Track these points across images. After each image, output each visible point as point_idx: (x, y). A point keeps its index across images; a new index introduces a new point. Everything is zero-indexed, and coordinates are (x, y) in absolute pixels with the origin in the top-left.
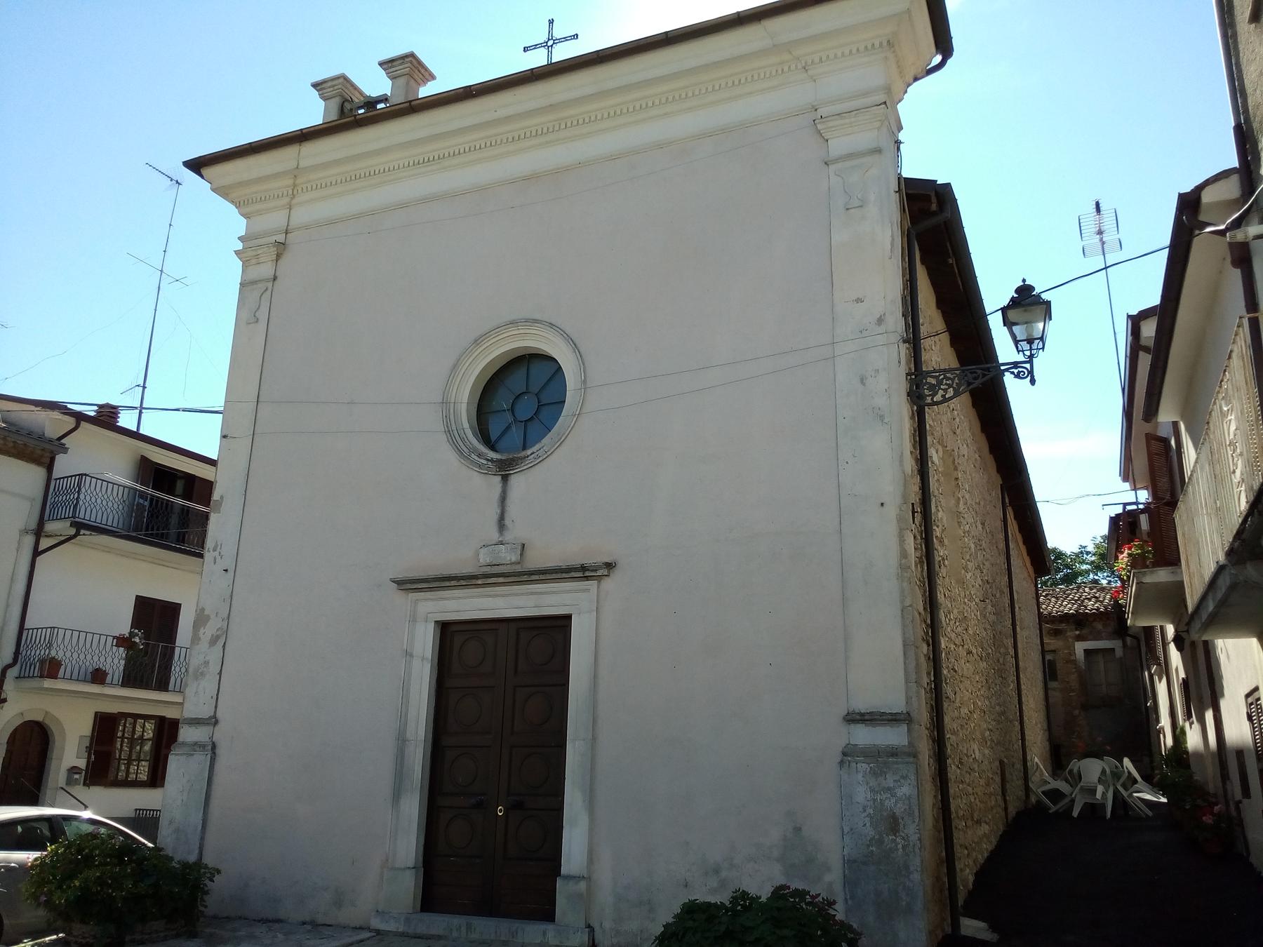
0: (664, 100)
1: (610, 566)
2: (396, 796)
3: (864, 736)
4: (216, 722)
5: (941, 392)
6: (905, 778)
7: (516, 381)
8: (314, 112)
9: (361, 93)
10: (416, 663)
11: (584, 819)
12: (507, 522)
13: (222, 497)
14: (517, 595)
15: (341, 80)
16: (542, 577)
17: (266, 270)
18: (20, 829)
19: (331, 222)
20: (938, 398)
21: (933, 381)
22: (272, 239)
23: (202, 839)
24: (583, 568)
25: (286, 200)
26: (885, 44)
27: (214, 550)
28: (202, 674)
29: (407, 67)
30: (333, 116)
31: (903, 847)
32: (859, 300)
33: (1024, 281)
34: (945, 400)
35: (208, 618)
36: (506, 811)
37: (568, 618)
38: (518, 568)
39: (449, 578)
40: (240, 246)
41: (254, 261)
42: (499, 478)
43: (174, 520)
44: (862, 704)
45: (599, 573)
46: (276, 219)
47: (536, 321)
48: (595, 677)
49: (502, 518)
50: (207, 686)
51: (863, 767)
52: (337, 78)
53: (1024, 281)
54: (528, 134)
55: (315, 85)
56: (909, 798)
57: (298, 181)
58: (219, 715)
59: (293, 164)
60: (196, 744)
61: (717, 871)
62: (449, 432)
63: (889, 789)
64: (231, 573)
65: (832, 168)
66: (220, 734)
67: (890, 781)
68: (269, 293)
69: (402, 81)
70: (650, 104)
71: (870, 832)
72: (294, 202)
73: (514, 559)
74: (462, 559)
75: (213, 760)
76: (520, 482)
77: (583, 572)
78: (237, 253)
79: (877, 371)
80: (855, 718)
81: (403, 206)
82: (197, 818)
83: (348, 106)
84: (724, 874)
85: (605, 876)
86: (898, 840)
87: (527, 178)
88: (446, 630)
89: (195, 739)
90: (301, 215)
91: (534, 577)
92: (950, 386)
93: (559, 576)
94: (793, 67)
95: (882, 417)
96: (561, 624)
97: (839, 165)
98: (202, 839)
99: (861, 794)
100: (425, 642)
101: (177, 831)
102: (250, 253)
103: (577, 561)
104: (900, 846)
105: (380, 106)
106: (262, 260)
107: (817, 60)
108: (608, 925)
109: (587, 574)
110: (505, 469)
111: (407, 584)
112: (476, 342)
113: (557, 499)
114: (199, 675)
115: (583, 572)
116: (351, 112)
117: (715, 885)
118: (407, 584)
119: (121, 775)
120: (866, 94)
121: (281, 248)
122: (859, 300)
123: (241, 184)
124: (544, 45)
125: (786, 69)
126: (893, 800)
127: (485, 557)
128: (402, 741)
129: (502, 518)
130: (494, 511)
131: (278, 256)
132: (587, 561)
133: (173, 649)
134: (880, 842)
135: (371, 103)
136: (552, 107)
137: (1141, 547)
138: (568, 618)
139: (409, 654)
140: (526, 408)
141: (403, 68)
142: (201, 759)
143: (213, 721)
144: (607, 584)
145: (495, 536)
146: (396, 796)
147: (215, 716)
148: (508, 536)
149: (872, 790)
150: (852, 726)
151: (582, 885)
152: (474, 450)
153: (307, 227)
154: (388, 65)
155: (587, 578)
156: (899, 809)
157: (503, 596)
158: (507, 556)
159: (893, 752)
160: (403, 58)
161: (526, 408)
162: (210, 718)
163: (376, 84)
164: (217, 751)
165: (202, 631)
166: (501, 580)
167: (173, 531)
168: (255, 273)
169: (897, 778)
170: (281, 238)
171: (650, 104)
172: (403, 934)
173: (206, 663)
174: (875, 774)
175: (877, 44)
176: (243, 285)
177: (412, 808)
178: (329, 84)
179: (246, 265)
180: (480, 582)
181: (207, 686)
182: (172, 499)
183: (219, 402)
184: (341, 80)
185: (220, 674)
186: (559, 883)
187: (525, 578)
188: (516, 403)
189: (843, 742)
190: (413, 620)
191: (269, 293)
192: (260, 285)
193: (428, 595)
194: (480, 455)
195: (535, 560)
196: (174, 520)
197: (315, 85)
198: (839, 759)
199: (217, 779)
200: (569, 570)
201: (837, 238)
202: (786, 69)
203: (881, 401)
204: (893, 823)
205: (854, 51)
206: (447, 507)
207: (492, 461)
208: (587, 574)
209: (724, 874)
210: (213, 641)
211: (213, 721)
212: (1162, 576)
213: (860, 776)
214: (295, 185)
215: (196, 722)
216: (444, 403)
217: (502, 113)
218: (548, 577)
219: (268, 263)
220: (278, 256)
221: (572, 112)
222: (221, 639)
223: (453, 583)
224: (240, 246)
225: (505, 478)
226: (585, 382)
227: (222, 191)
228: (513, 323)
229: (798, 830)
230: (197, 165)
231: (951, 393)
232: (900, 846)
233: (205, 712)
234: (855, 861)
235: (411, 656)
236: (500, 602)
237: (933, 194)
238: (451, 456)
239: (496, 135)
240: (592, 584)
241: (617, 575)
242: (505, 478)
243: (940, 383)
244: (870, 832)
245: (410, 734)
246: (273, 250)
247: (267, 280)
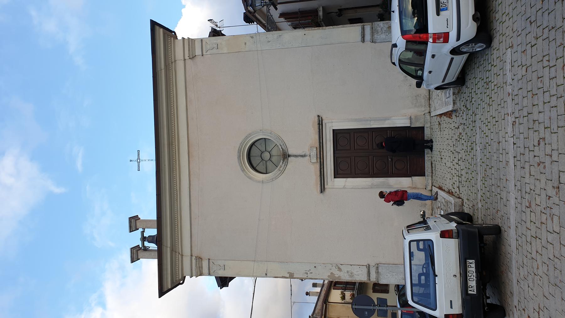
1: (318, 116)
3: (368, 37)
7: (255, 151)
12: (303, 154)
18: (366, 313)
24: (319, 124)
32: (245, 44)
38: (318, 148)
44: (359, 38)
49: (302, 156)
51: (376, 36)
65: (204, 53)
77: (320, 123)
80: (363, 40)
88: (337, 175)
89: (374, 273)
100: (341, 182)
108: (423, 109)
110: (286, 156)
111: (323, 189)
114: (352, 275)
115: (320, 123)
118: (323, 189)
119: (348, 294)
127: (314, 160)
129: (302, 156)
130: (300, 159)
139: (344, 188)
145: (308, 158)
148: (308, 153)
172: (432, 177)
174: (378, 33)
186: (413, 126)
201: (225, 52)
203: (275, 36)
210: (340, 269)
211: (368, 267)
225: (289, 156)
233: (365, 270)
236: (328, 143)
242: (289, 156)
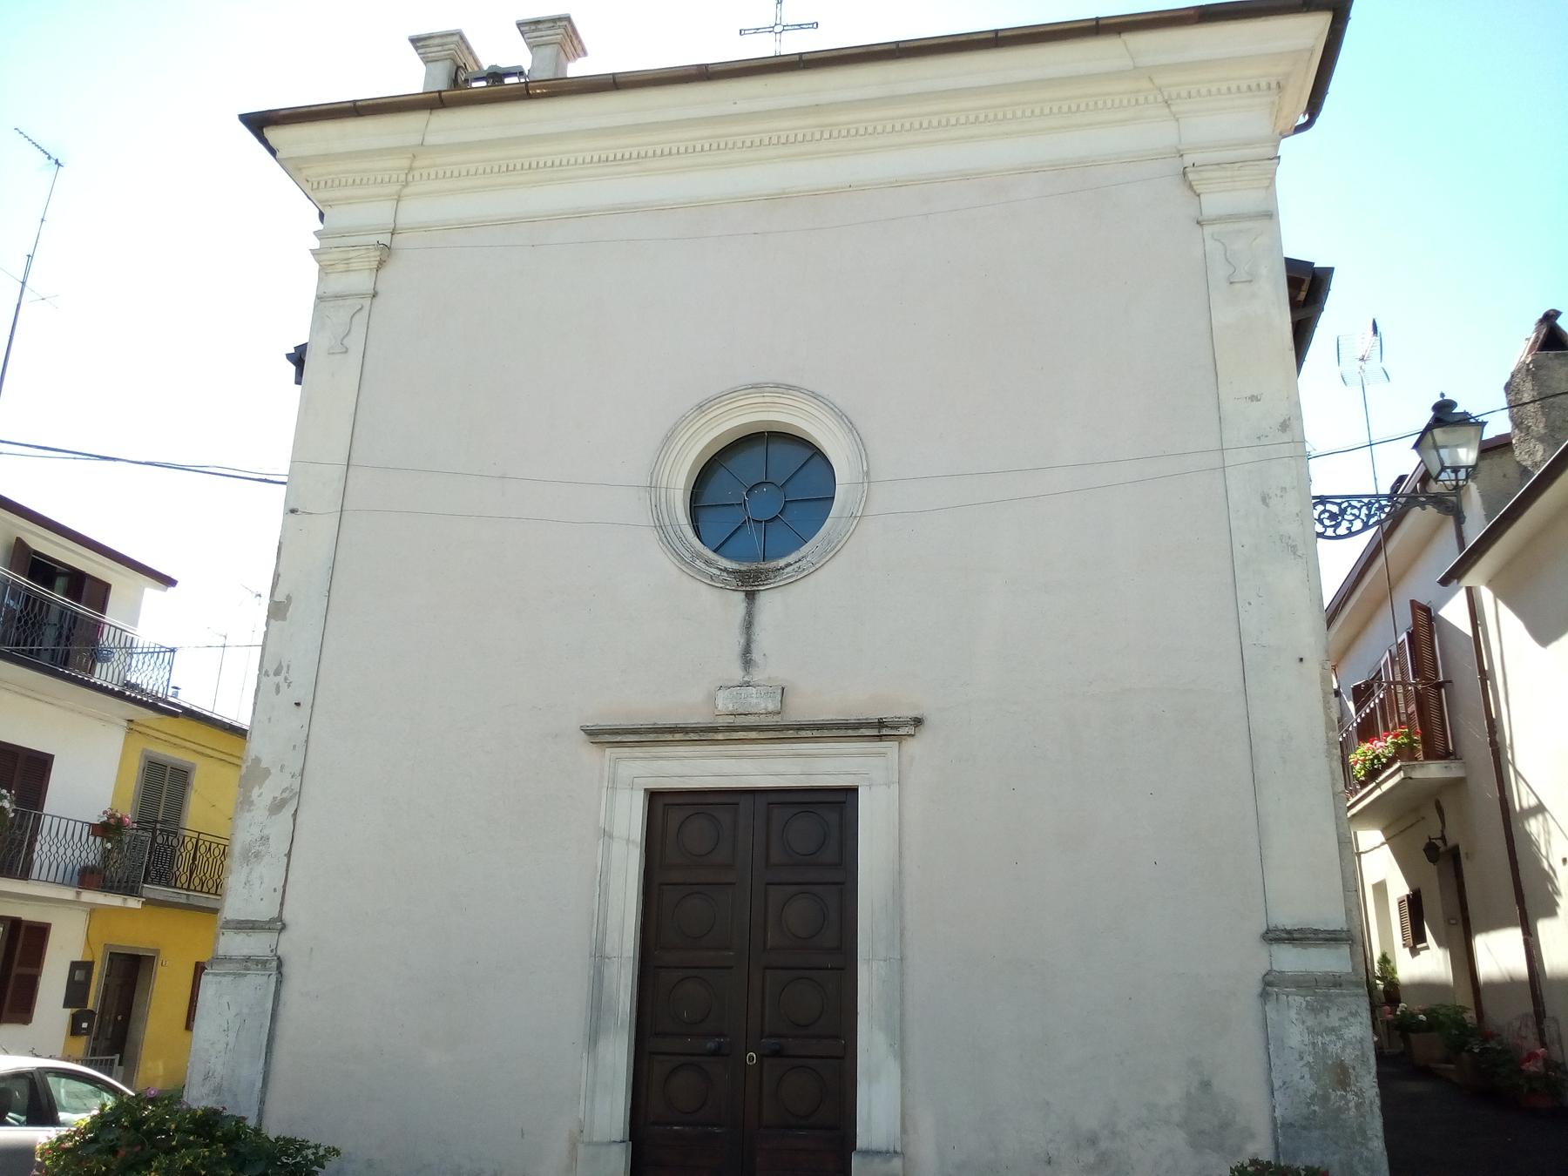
0: (972, 119)
1: (918, 722)
2: (593, 1037)
3: (1291, 960)
4: (284, 927)
5: (1345, 524)
6: (1354, 1014)
8: (411, 78)
9: (476, 61)
10: (618, 848)
11: (892, 1068)
12: (756, 655)
13: (289, 598)
14: (775, 756)
15: (456, 38)
16: (816, 733)
17: (360, 281)
19: (465, 226)
20: (1342, 530)
21: (1335, 509)
22: (373, 239)
23: (262, 1102)
24: (881, 724)
25: (395, 188)
26: (1274, 85)
27: (277, 673)
28: (257, 855)
29: (552, 32)
30: (441, 84)
31: (1358, 1106)
32: (1254, 398)
33: (1442, 395)
34: (1351, 534)
35: (267, 772)
36: (761, 1057)
37: (852, 791)
39: (673, 730)
40: (316, 244)
41: (341, 267)
42: (742, 595)
43: (50, 633)
44: (1286, 919)
45: (902, 731)
46: (377, 213)
47: (790, 387)
48: (900, 873)
50: (268, 872)
51: (1297, 1000)
52: (452, 34)
53: (1442, 395)
54: (774, 140)
55: (415, 41)
56: (1361, 1041)
57: (417, 164)
58: (287, 916)
59: (414, 139)
60: (248, 959)
61: (1093, 1141)
62: (661, 527)
63: (1333, 1029)
64: (306, 708)
65: (1208, 230)
66: (287, 945)
67: (1333, 1019)
68: (365, 312)
69: (548, 51)
70: (953, 121)
71: (1310, 1087)
72: (407, 191)
73: (771, 707)
74: (688, 705)
75: (279, 982)
76: (771, 602)
77: (881, 729)
78: (314, 253)
79: (1284, 489)
80: (1276, 936)
81: (581, 214)
82: (251, 1071)
83: (462, 77)
84: (1104, 1145)
85: (925, 1149)
86: (1350, 1096)
87: (771, 198)
89: (246, 952)
90: (415, 211)
91: (803, 734)
92: (1357, 517)
93: (842, 733)
94: (1151, 98)
95: (1294, 549)
96: (842, 800)
97: (1216, 228)
98: (262, 1102)
99: (1296, 1036)
100: (631, 819)
101: (218, 1090)
102: (336, 255)
103: (874, 715)
104: (1352, 1104)
105: (508, 81)
106: (354, 266)
107: (1184, 94)
109: (884, 732)
110: (750, 583)
111: (601, 736)
112: (701, 408)
113: (829, 628)
115: (881, 729)
116: (462, 86)
117: (1092, 1160)
118: (601, 736)
120: (1248, 143)
121: (386, 253)
122: (1254, 398)
123: (326, 157)
124: (771, 30)
125: (1141, 100)
126: (1340, 1044)
127: (725, 703)
128: (599, 959)
130: (735, 641)
131: (381, 264)
132: (887, 714)
133: (38, 819)
134: (1325, 1099)
135: (496, 76)
136: (817, 108)
137: (1408, 736)
138: (852, 791)
139: (607, 835)
140: (765, 503)
141: (556, 35)
142: (257, 985)
143: (278, 925)
144: (911, 746)
145: (738, 674)
146: (593, 1037)
147: (280, 918)
148: (757, 676)
149: (1311, 1031)
150: (1275, 947)
151: (897, 1163)
152: (699, 556)
153: (426, 228)
154: (530, 28)
155: (880, 738)
156: (1349, 1056)
157: (752, 757)
158: (760, 703)
159: (1336, 982)
160: (560, 19)
161: (765, 503)
162: (272, 921)
163: (499, 48)
164: (285, 970)
165: (256, 792)
166: (753, 735)
167: (48, 644)
168: (339, 283)
169: (1343, 1014)
170: (385, 239)
171: (953, 121)
173: (265, 839)
174: (1313, 1009)
175: (1263, 85)
176: (320, 299)
177: (617, 1053)
178: (437, 41)
179: (324, 271)
180: (720, 736)
181: (268, 872)
182: (67, 601)
183: (279, 463)
184: (456, 38)
185: (289, 855)
186: (856, 1161)
187: (791, 734)
188: (758, 497)
189: (1263, 968)
190: (613, 786)
191: (365, 312)
192: (349, 302)
193: (638, 752)
194: (707, 562)
195: (801, 710)
196: (50, 633)
197: (415, 41)
198: (1259, 990)
199: (283, 1012)
200: (847, 726)
202: (1141, 100)
204: (1342, 1076)
205: (1234, 89)
206: (665, 631)
207: (734, 572)
208: (884, 732)
209: (1104, 1145)
210: (277, 806)
211: (278, 925)
212: (1434, 771)
213: (1293, 1014)
214: (411, 169)
215: (247, 926)
216: (652, 487)
217: (744, 107)
218: (826, 733)
219: (362, 268)
220: (381, 264)
221: (843, 118)
222: (288, 803)
223: (678, 736)
224: (316, 244)
225: (751, 596)
226: (867, 474)
227: (293, 167)
228: (756, 387)
229: (1206, 1085)
230: (258, 123)
231: (1358, 525)
232: (1352, 1104)
233: (264, 910)
234: (1291, 1125)
235: (611, 837)
237: (1308, 280)
238: (666, 564)
239: (936, 114)
240: (890, 747)
241: (925, 735)
242: (751, 596)
243: (1343, 512)
244: (1310, 1087)
245: (611, 946)
246: (375, 255)
247: (362, 296)
